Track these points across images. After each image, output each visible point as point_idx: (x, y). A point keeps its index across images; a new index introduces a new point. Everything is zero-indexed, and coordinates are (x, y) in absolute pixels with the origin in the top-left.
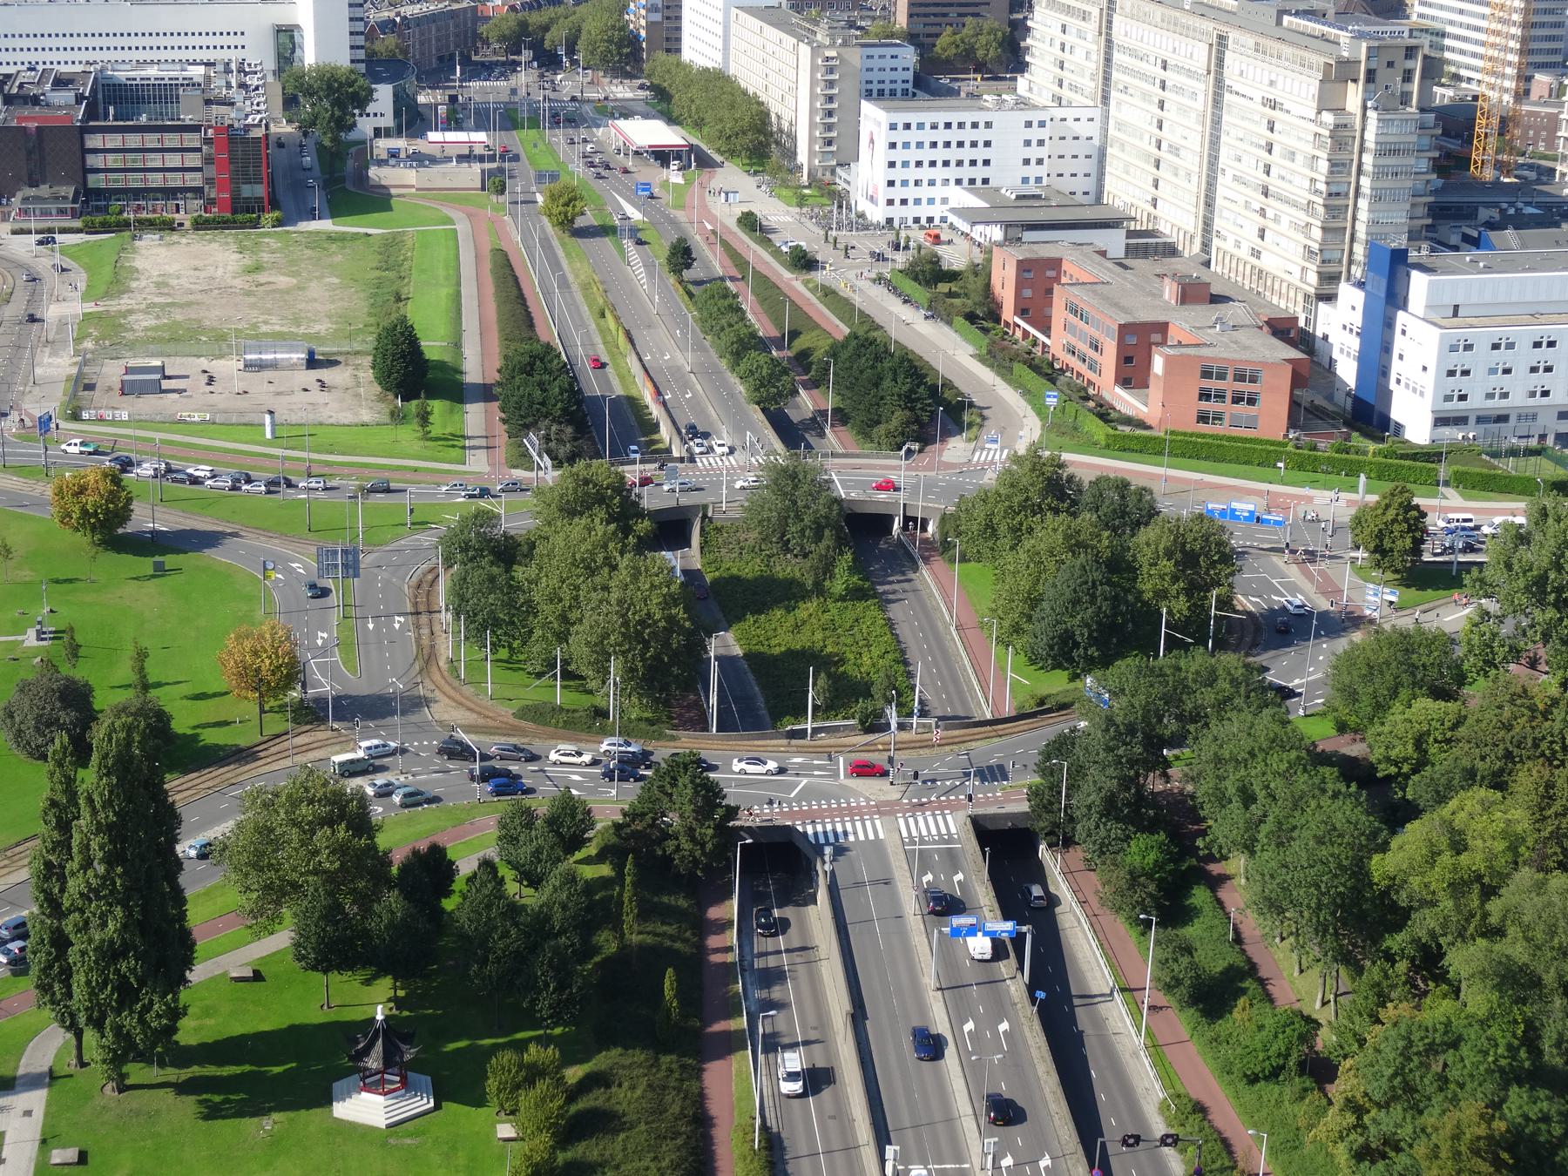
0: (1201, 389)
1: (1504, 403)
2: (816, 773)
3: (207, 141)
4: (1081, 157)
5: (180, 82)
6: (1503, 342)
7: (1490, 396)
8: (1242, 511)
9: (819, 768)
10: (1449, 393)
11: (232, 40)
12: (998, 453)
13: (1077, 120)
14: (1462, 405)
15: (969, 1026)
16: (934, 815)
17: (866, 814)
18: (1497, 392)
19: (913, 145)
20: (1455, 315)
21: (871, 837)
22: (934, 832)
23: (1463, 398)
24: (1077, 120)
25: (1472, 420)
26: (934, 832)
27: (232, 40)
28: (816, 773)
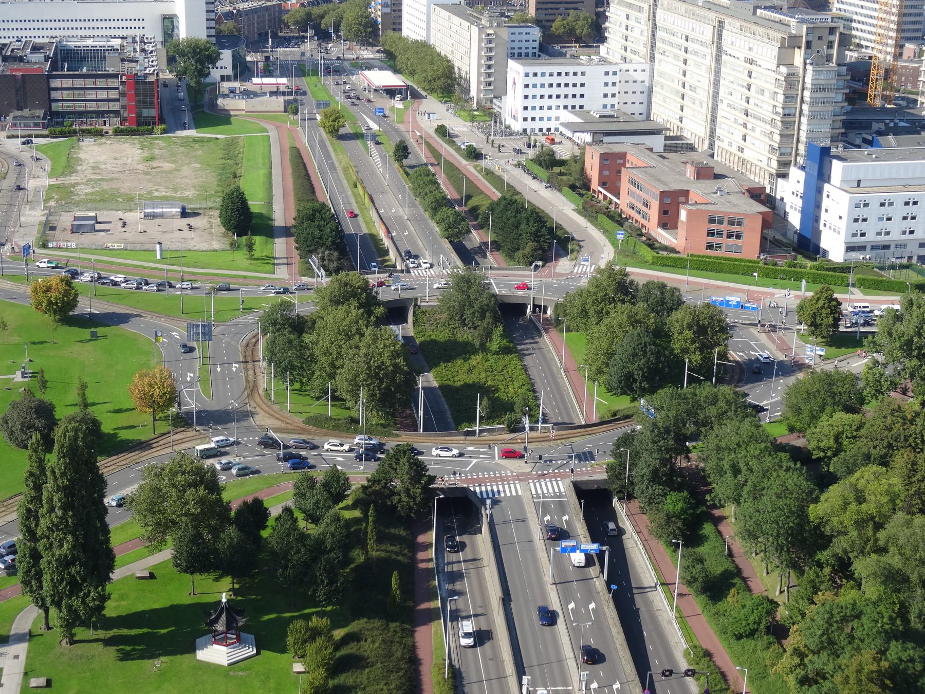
0: (709, 230)
1: (887, 238)
2: (481, 456)
3: (122, 83)
4: (638, 93)
5: (106, 48)
6: (887, 202)
7: (879, 234)
8: (733, 301)
9: (483, 453)
10: (855, 232)
11: (137, 24)
12: (589, 267)
13: (636, 71)
14: (863, 239)
15: (572, 606)
16: (551, 481)
17: (511, 480)
18: (883, 231)
19: (539, 86)
20: (859, 186)
21: (514, 494)
22: (551, 491)
23: (863, 235)
24: (636, 71)
25: (869, 248)
26: (551, 491)
27: (137, 24)
28: (481, 456)
